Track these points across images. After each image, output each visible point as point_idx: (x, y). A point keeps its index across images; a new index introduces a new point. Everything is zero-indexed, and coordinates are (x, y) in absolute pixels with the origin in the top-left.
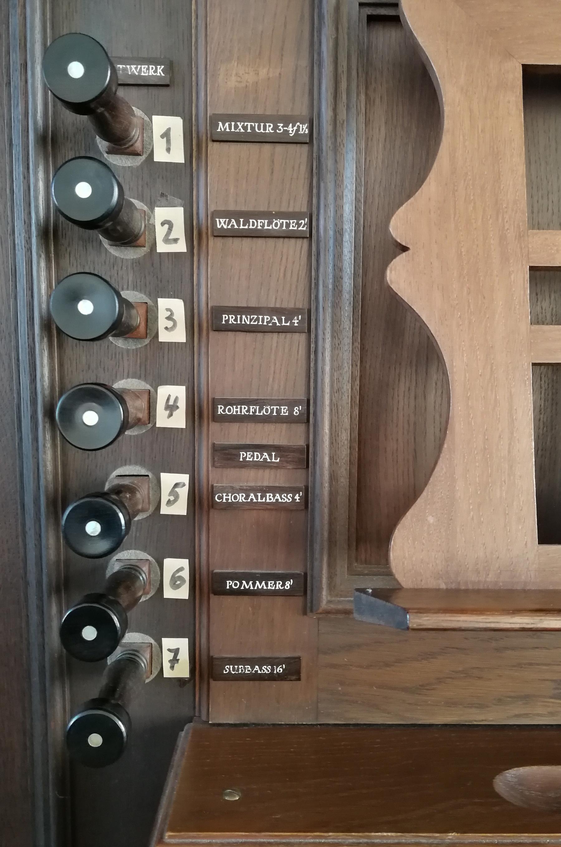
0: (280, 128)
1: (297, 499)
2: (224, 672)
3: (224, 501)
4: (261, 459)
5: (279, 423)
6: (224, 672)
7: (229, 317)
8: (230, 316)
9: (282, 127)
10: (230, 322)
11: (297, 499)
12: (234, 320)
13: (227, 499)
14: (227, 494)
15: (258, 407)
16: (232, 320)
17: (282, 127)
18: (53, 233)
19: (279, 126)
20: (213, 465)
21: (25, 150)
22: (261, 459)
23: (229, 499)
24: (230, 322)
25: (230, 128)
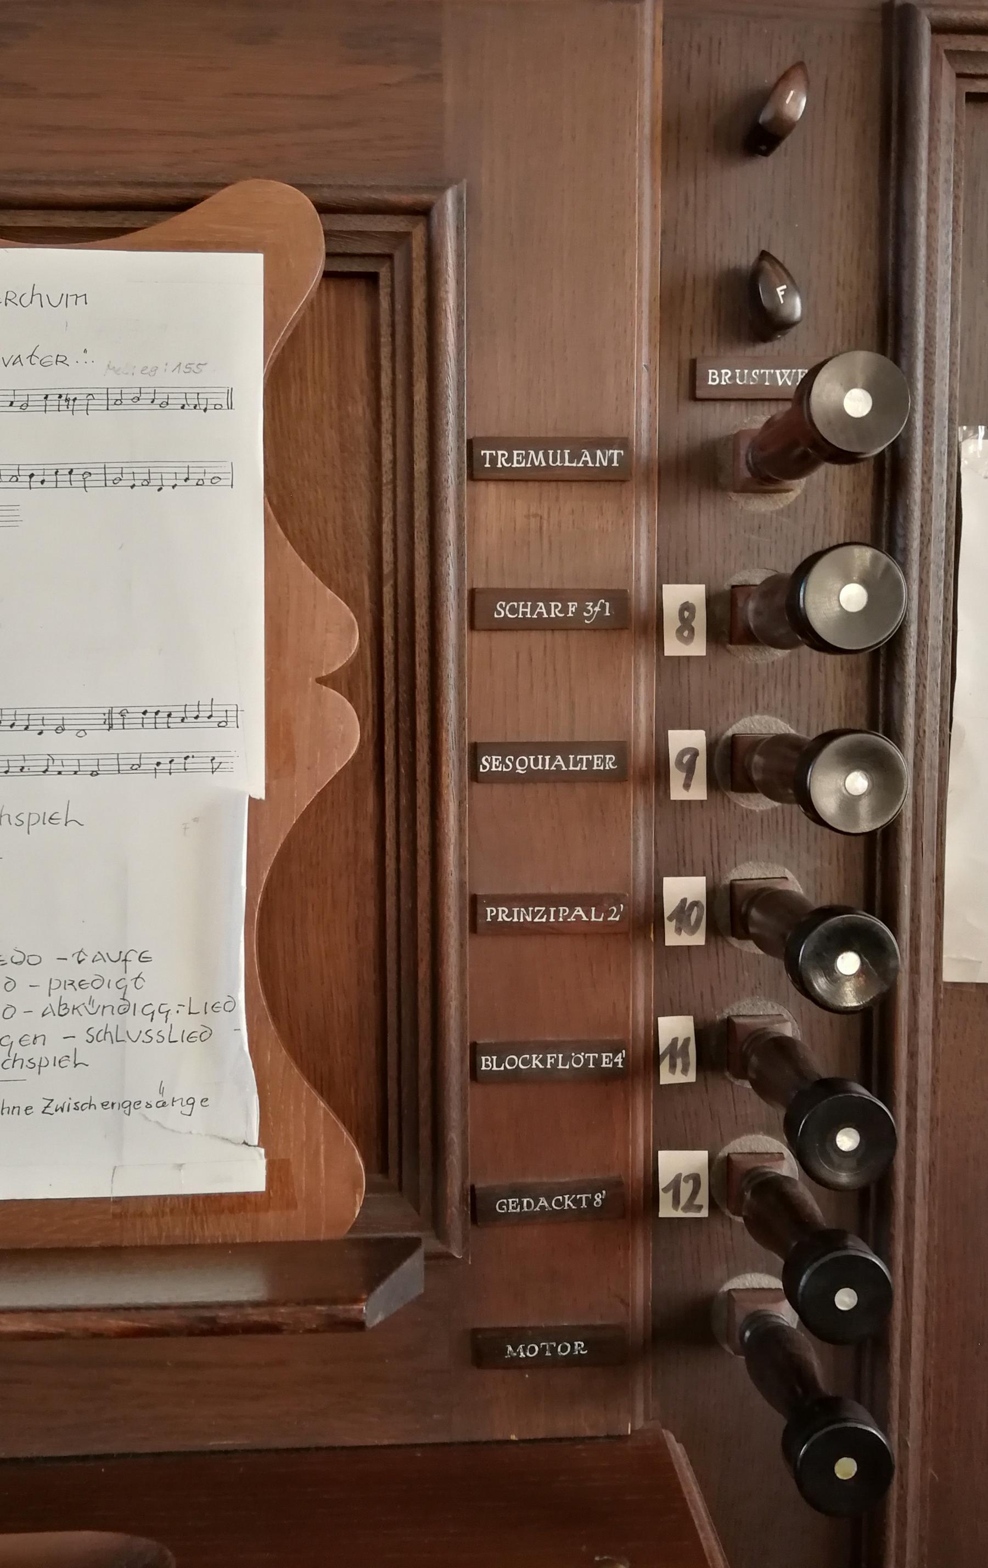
0: (589, 608)
1: (620, 1063)
2: (496, 616)
3: (520, 616)
4: (535, 1207)
5: (569, 589)
6: (496, 616)
7: (497, 911)
8: (500, 909)
9: (592, 607)
10: (500, 919)
11: (620, 1063)
12: (559, 611)
13: (524, 613)
14: (524, 617)
15: (560, 1056)
16: (557, 610)
17: (592, 607)
18: (605, 608)
19: (589, 605)
20: (472, 627)
21: (925, 1199)
22: (535, 1207)
23: (527, 612)
24: (500, 919)
25: (547, 461)
